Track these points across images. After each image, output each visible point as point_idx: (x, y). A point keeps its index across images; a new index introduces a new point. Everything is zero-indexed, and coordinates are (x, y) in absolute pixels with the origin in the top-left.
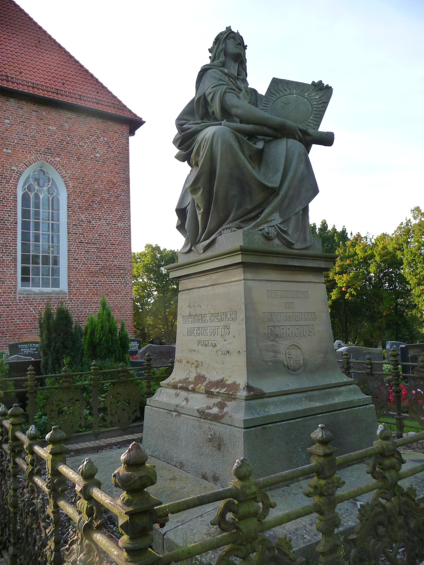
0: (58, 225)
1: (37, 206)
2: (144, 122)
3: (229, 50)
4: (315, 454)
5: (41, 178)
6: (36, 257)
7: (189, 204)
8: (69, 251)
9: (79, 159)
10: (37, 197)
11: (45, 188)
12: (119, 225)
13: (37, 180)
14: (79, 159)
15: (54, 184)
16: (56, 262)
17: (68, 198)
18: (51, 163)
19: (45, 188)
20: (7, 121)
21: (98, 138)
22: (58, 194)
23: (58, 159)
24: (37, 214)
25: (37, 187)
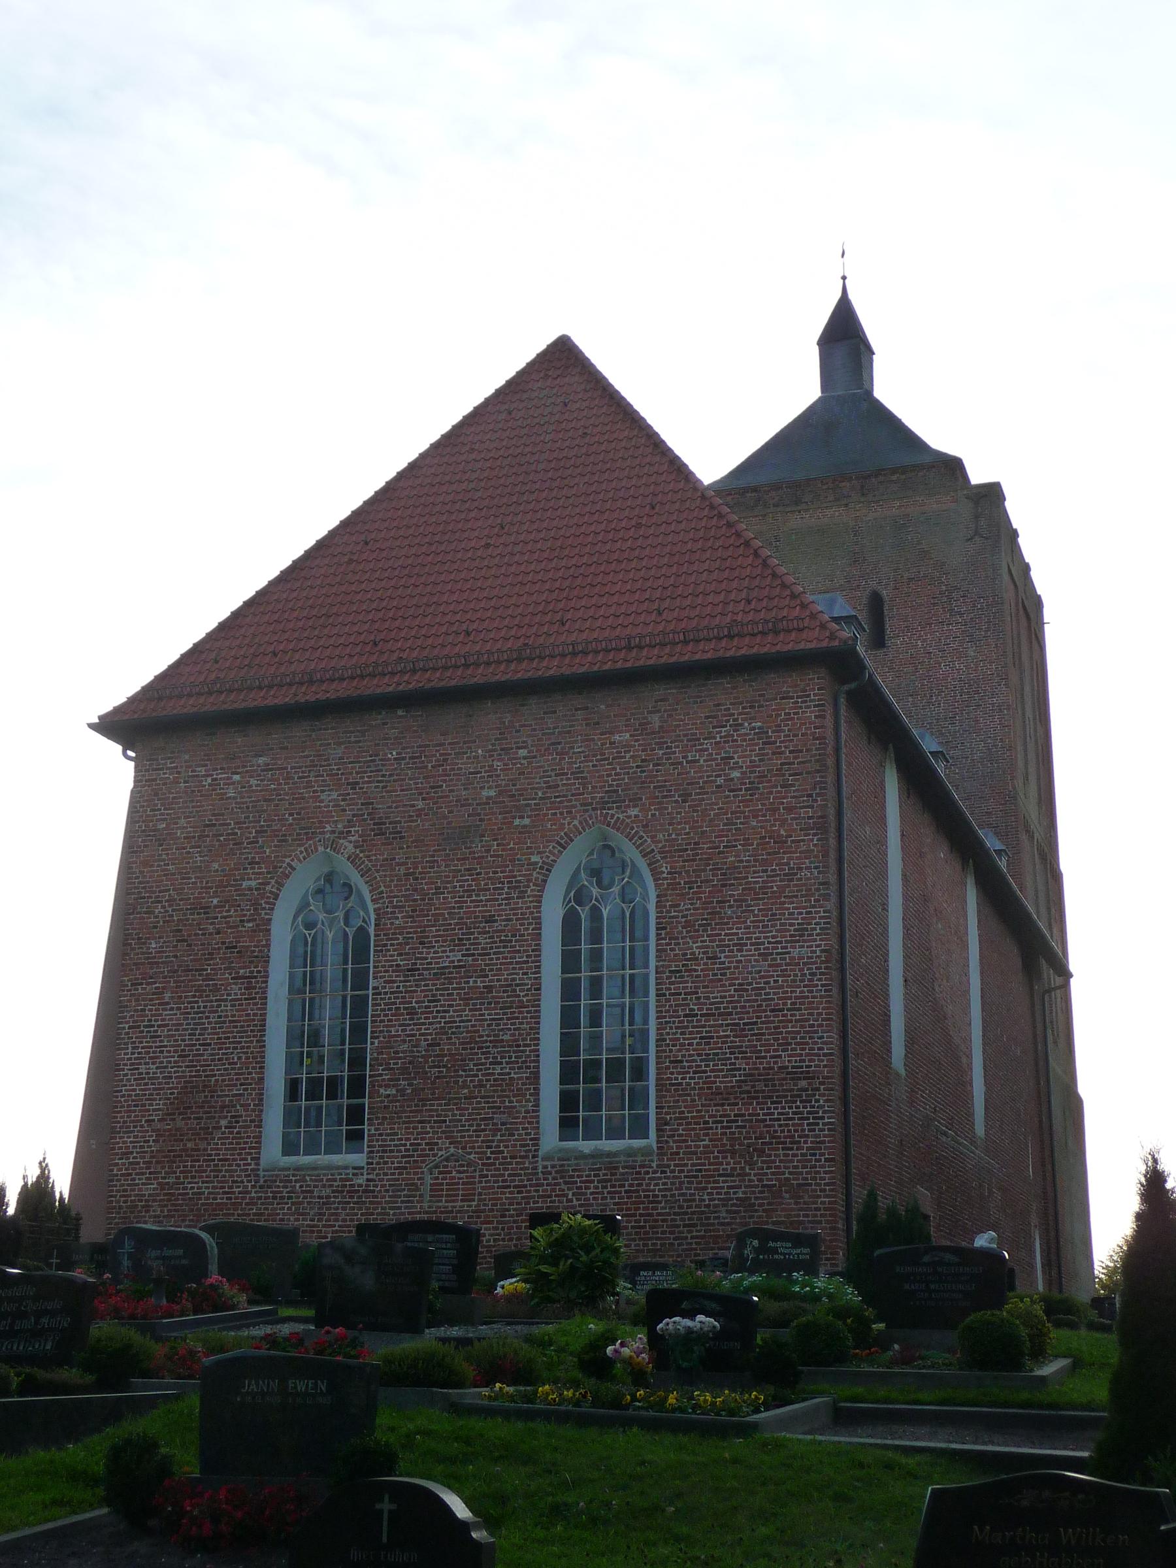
10: (596, 914)
11: (616, 889)
12: (795, 953)
13: (596, 873)
14: (685, 797)
19: (616, 889)
20: (523, 752)
21: (737, 726)
23: (633, 812)
25: (595, 891)
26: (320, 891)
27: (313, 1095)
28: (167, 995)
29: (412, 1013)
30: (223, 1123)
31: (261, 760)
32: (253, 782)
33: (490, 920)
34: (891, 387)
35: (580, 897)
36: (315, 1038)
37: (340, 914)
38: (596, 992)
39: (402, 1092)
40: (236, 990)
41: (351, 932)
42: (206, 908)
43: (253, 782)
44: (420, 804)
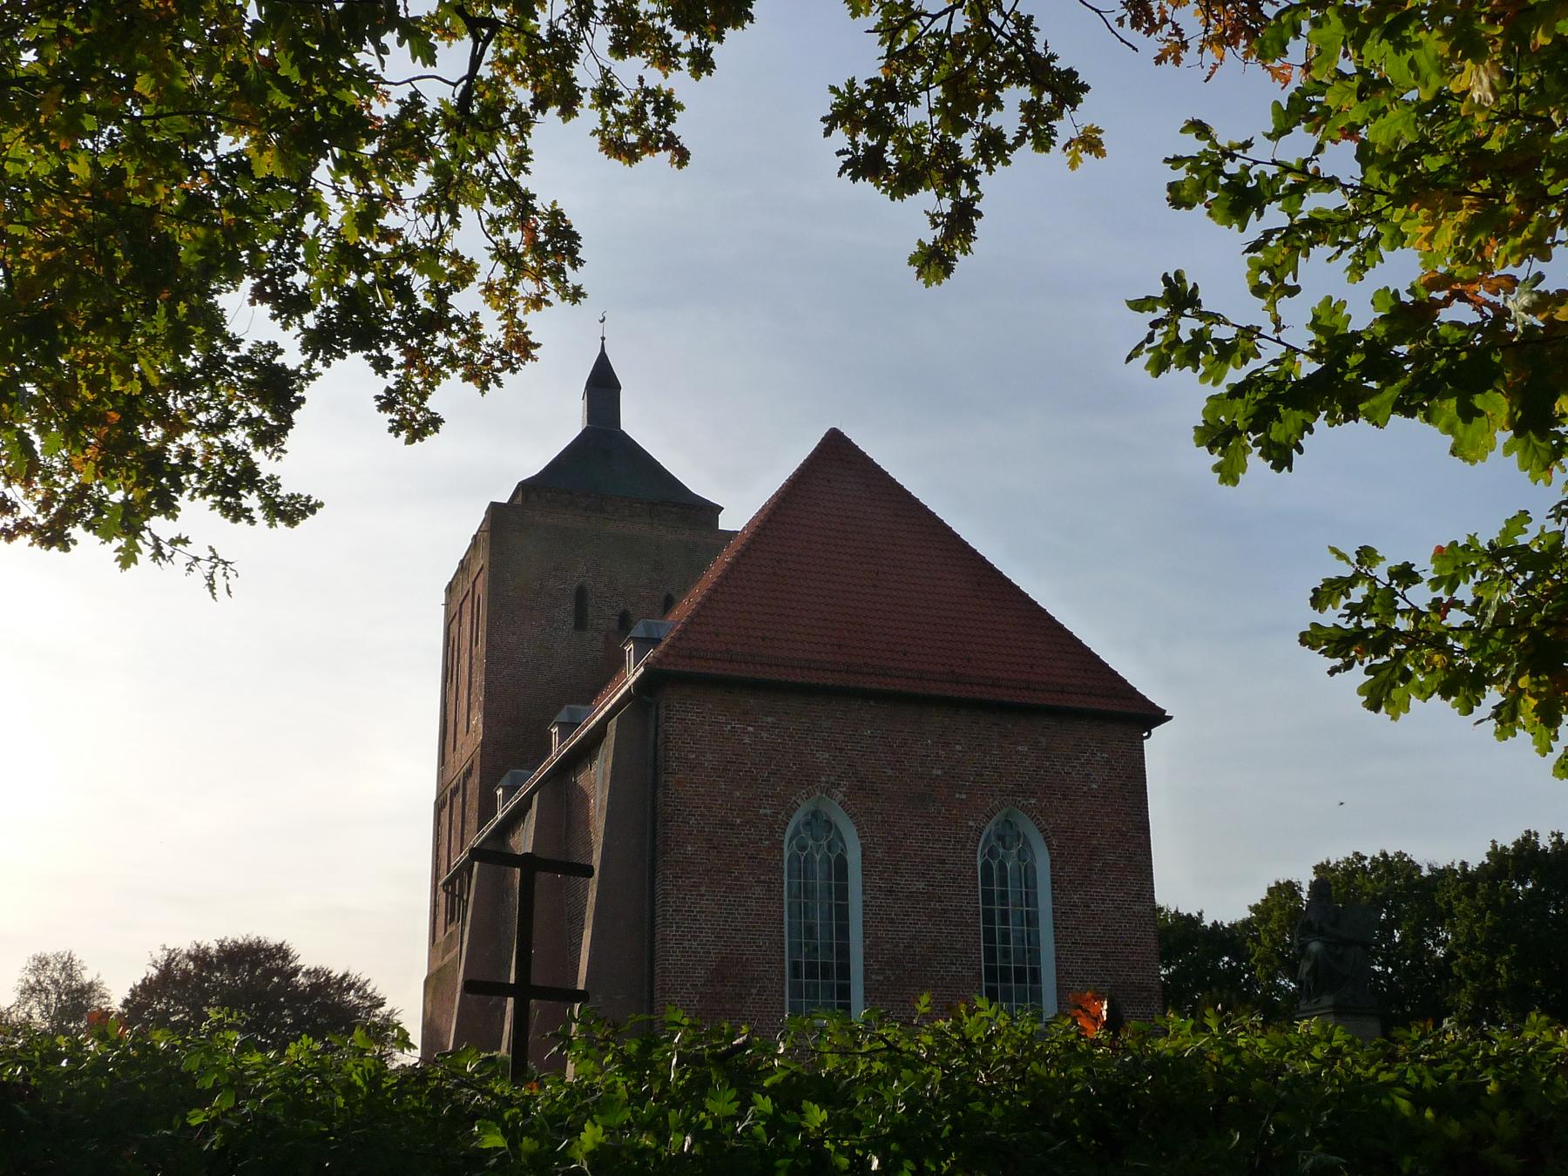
0: (1036, 914)
1: (1003, 882)
2: (1170, 718)
3: (1290, 470)
4: (1210, 138)
5: (1008, 833)
6: (1005, 971)
7: (469, 772)
8: (1057, 958)
9: (1065, 797)
10: (1002, 867)
11: (1014, 851)
12: (1136, 908)
13: (1001, 838)
14: (1065, 797)
15: (1027, 842)
16: (1036, 976)
17: (1052, 866)
18: (1025, 809)
19: (1014, 851)
20: (958, 748)
21: (1093, 754)
22: (844, 850)
23: (1033, 801)
24: (1004, 895)
25: (1001, 850)
26: (808, 824)
27: (811, 974)
28: (703, 889)
29: (892, 922)
30: (754, 991)
31: (770, 719)
32: (764, 735)
33: (943, 862)
34: (635, 422)
35: (992, 853)
36: (810, 931)
37: (824, 843)
38: (1005, 920)
39: (888, 978)
40: (758, 891)
41: (833, 857)
42: (732, 826)
43: (764, 735)
44: (890, 772)
